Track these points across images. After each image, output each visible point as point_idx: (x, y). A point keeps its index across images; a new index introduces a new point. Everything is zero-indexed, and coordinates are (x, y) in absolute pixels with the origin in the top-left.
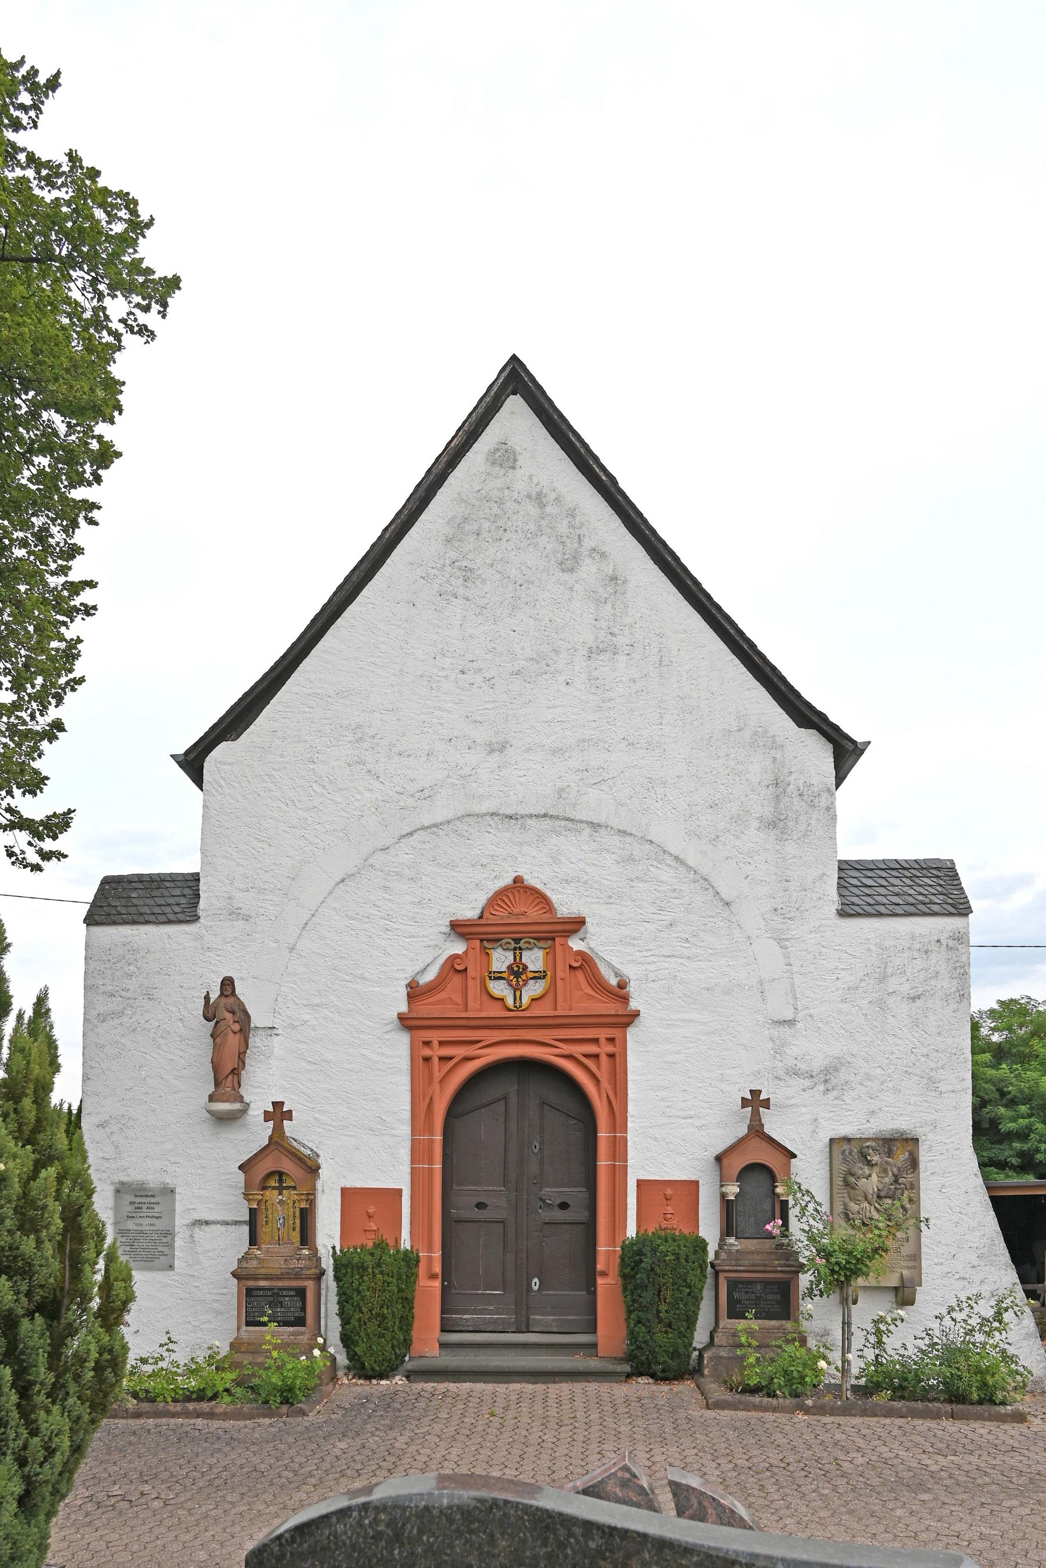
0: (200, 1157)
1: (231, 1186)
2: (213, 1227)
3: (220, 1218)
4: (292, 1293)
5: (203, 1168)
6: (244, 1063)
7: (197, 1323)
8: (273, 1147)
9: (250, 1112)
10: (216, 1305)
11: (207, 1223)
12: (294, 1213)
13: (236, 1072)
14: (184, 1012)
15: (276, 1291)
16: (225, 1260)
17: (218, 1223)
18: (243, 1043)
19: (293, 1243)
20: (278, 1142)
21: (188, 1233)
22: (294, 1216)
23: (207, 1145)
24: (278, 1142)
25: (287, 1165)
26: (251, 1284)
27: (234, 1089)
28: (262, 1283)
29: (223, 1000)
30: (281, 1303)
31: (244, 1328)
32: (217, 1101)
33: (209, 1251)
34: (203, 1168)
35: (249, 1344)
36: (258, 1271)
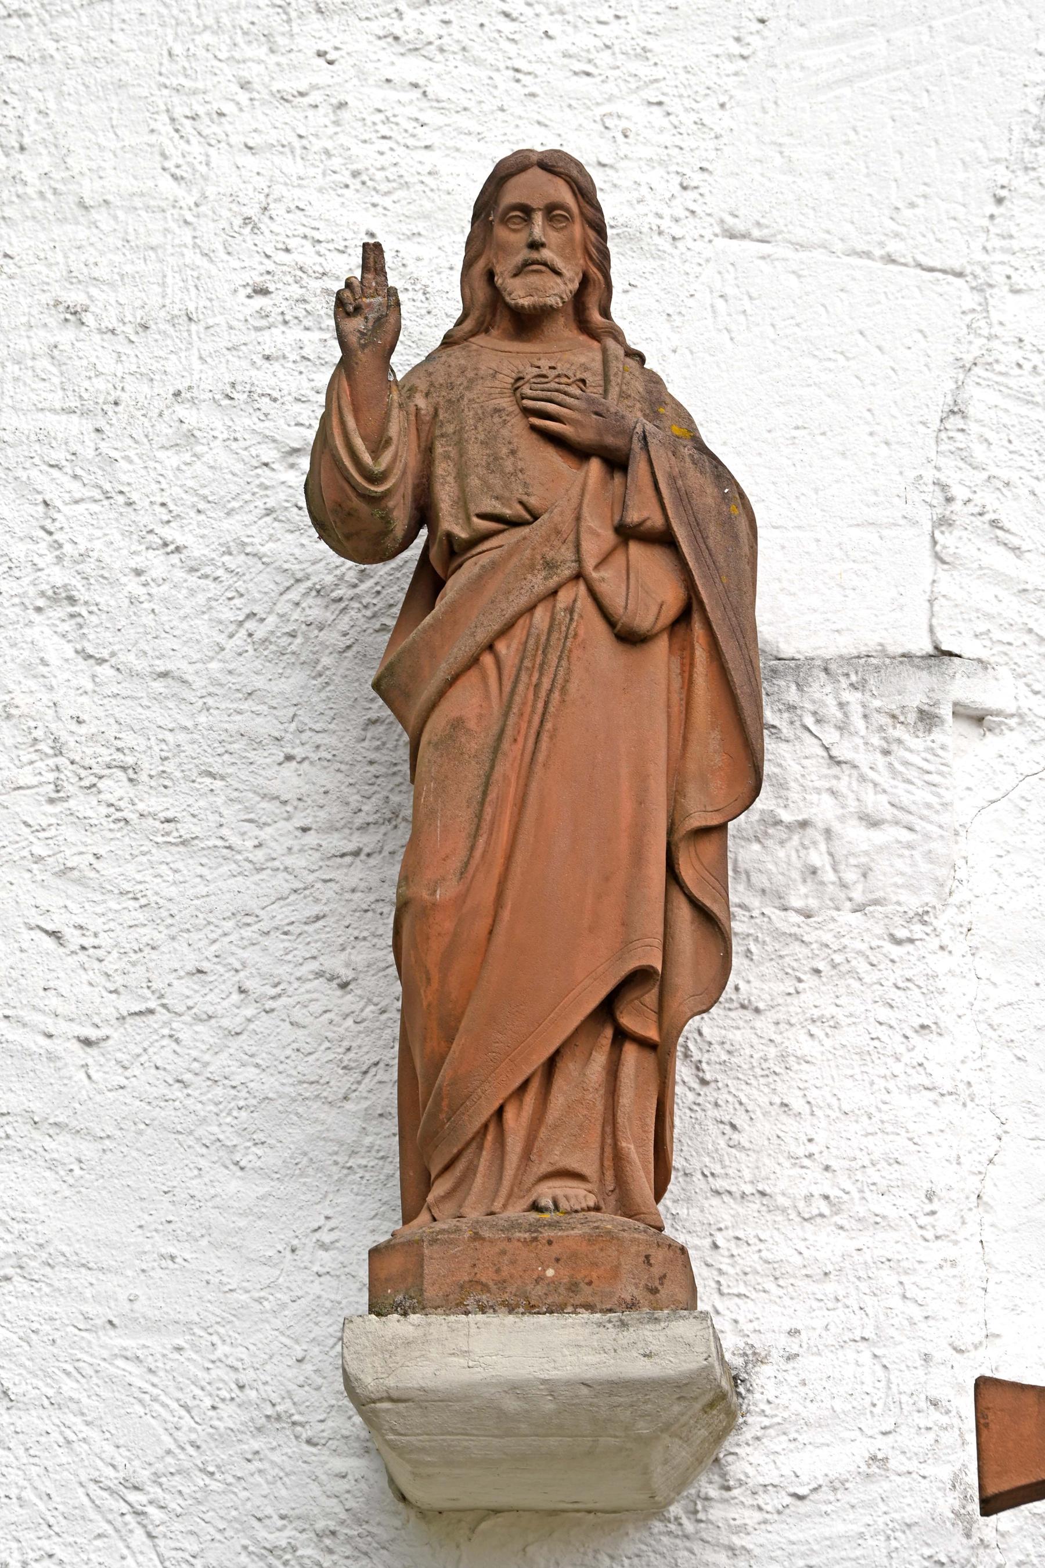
6: (713, 925)
9: (750, 1457)
13: (636, 1019)
14: (88, 528)
18: (709, 743)
27: (627, 1207)
29: (501, 357)
32: (470, 1296)
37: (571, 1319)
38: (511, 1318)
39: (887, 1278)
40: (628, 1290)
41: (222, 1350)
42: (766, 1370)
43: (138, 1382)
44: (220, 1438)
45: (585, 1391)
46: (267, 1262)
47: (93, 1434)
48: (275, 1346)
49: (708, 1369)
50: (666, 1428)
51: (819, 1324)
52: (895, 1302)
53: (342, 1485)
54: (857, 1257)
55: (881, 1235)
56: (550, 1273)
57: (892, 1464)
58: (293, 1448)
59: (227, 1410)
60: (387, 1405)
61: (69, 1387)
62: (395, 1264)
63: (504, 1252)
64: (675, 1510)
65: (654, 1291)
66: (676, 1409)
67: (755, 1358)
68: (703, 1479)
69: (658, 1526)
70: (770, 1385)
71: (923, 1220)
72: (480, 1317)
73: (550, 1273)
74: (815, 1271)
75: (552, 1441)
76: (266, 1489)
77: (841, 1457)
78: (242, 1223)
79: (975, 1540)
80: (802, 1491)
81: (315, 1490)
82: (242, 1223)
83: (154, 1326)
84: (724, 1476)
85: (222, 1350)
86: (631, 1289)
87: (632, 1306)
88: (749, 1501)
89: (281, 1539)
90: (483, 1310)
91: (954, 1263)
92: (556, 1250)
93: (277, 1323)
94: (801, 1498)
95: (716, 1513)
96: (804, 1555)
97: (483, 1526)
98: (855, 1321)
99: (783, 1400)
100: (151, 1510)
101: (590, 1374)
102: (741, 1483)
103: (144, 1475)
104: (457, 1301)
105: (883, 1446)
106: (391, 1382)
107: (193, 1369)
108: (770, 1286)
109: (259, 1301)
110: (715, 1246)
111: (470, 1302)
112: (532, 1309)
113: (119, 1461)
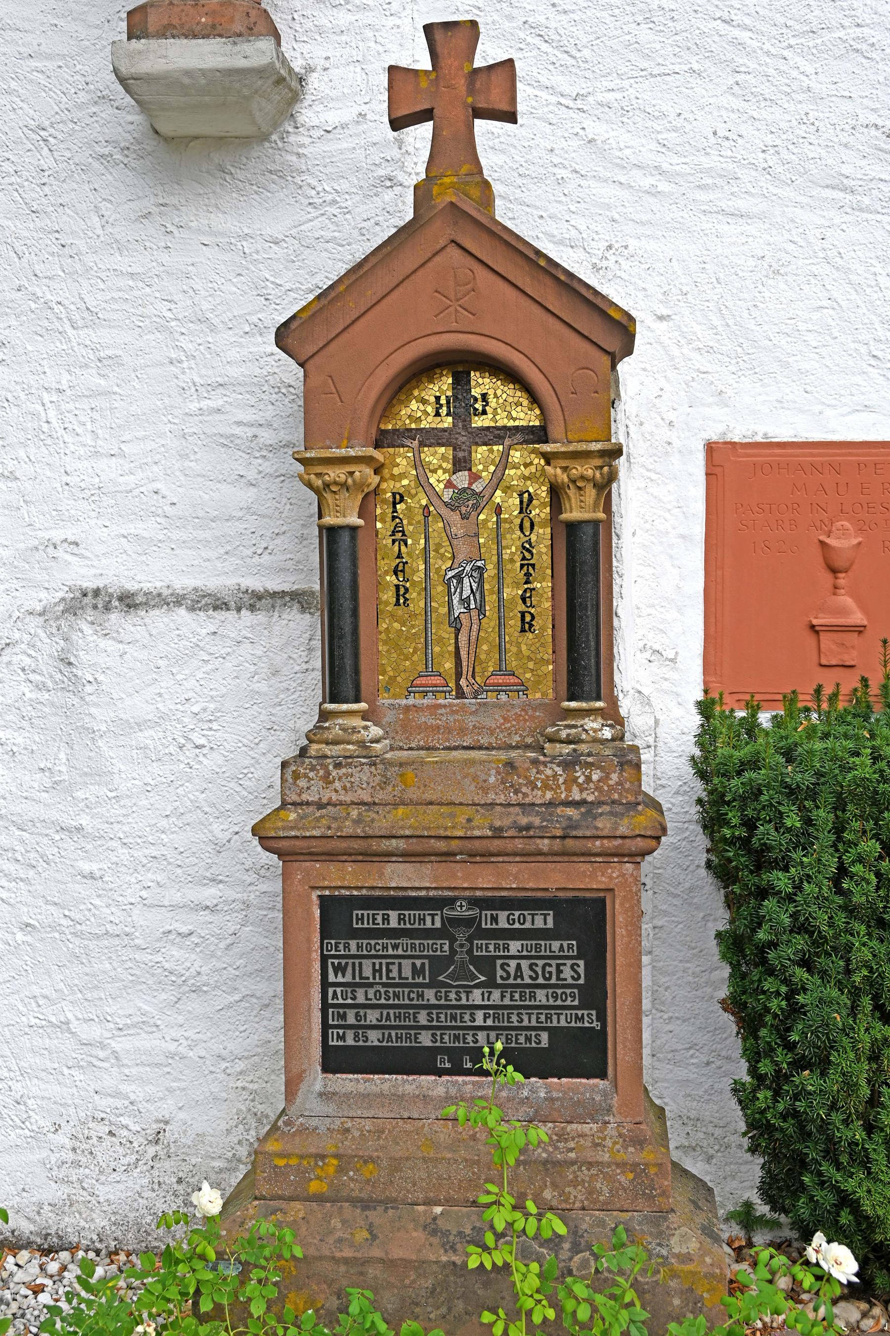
0: (93, 317)
1: (228, 442)
2: (158, 619)
3: (184, 582)
4: (543, 921)
5: (107, 362)
7: (95, 1032)
8: (440, 232)
10: (176, 956)
11: (129, 602)
12: (527, 549)
15: (462, 911)
16: (211, 762)
17: (178, 600)
19: (523, 688)
20: (453, 210)
21: (50, 646)
22: (527, 566)
23: (120, 262)
24: (453, 210)
25: (502, 322)
26: (347, 878)
28: (399, 877)
30: (487, 965)
31: (317, 1080)
32: (165, 32)
33: (141, 725)
34: (107, 362)
35: (344, 1161)
36: (382, 822)
37: (212, 41)
38: (186, 41)
39: (369, 34)
40: (238, 27)
41: (79, 67)
42: (315, 75)
43: (43, 82)
44: (80, 107)
45: (218, 74)
46: (97, 27)
47: (25, 106)
48: (102, 65)
49: (272, 64)
50: (256, 92)
51: (338, 54)
52: (372, 44)
53: (131, 127)
54: (356, 24)
55: (367, 14)
56: (203, 20)
57: (368, 117)
58: (110, 111)
59: (81, 94)
60: (132, 81)
61: (13, 85)
62: (137, 18)
63: (183, 11)
64: (274, 137)
65: (251, 29)
66: (259, 83)
67: (310, 69)
68: (286, 124)
69: (267, 145)
70: (316, 81)
71: (385, 7)
72: (172, 40)
73: (203, 20)
74: (337, 30)
75: (207, 98)
76: (99, 129)
77: (347, 114)
78: (86, 9)
79: (403, 151)
80: (329, 129)
81: (120, 129)
82: (86, 9)
83: (49, 57)
84: (295, 122)
85: (79, 67)
86: (240, 27)
87: (240, 35)
88: (306, 133)
89: (106, 151)
90: (174, 37)
91: (398, 27)
92: (206, 9)
93: (102, 55)
94: (328, 132)
95: (292, 139)
96: (329, 157)
97: (192, 144)
98: (354, 53)
99: (322, 89)
100: (50, 139)
101: (220, 66)
102: (303, 126)
103: (47, 123)
104: (162, 34)
105: (364, 109)
106: (133, 70)
107: (66, 76)
108: (318, 37)
109: (94, 45)
110: (294, 19)
111: (168, 34)
112: (195, 36)
113: (36, 117)
